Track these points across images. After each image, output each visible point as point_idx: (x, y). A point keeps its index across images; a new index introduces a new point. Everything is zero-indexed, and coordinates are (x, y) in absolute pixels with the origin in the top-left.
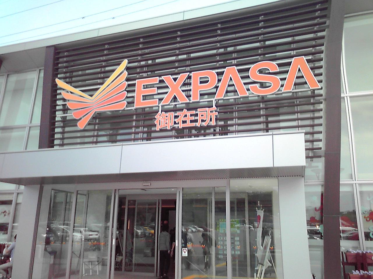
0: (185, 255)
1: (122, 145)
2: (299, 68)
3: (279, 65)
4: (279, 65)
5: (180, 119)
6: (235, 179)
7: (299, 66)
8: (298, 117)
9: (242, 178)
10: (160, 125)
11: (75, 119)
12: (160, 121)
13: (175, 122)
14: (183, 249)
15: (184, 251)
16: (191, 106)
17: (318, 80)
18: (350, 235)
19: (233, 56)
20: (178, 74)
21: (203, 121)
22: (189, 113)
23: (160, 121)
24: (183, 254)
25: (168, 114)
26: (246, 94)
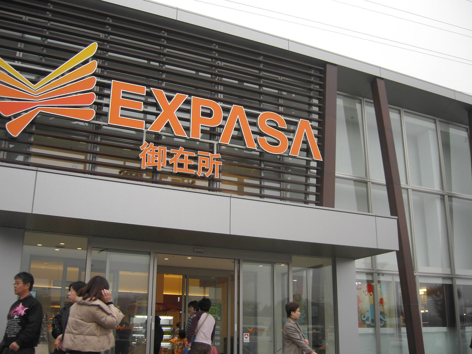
0: (247, 342)
1: (231, 197)
2: (238, 118)
3: (288, 122)
4: (288, 122)
5: (175, 160)
6: (53, 234)
8: (5, 146)
9: (85, 236)
10: (146, 162)
12: (147, 155)
13: (168, 162)
14: (244, 334)
15: (245, 336)
16: (192, 144)
17: (267, 140)
18: (464, 318)
19: (19, 46)
21: (204, 169)
22: (187, 154)
23: (147, 155)
24: (244, 340)
25: (158, 148)
26: (150, 129)
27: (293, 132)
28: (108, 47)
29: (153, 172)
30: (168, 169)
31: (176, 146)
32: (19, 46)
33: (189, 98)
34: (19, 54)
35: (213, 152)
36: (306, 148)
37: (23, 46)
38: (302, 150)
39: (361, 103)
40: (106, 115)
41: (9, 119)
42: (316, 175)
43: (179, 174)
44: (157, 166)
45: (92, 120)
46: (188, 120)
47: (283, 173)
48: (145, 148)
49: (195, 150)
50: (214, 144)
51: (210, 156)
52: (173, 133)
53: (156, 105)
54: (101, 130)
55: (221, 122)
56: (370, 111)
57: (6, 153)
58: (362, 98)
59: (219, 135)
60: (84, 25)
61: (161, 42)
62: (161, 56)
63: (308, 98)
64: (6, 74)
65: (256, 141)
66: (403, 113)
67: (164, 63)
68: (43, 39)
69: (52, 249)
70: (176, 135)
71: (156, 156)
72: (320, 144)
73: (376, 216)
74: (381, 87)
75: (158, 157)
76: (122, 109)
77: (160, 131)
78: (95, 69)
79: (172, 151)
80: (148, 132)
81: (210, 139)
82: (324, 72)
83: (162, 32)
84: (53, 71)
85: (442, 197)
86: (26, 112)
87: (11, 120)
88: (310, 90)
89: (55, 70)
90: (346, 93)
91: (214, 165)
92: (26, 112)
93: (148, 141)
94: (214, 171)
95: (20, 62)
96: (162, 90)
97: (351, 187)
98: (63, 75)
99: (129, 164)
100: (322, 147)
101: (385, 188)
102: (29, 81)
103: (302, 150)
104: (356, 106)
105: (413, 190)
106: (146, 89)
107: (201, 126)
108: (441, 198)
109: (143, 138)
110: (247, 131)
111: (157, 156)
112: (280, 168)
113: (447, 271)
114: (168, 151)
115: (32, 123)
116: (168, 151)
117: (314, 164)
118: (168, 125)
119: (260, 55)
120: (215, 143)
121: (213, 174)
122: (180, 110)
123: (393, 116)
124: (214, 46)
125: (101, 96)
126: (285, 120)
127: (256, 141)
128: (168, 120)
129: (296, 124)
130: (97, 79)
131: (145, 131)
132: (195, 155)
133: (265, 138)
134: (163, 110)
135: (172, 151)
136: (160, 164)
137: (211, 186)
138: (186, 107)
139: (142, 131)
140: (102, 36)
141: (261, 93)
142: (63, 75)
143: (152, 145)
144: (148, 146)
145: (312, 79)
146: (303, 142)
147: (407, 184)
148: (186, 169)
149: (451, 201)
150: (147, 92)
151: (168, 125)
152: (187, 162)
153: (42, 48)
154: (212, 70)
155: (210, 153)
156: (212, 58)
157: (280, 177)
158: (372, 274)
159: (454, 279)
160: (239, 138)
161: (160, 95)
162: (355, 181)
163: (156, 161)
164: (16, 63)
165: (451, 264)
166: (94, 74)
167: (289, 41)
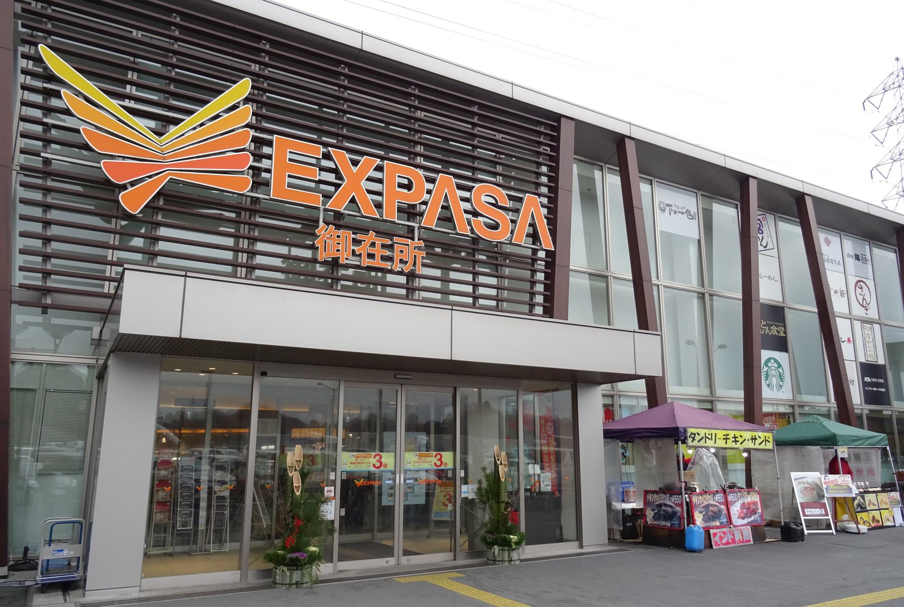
7: (446, 190)
10: (325, 251)
11: (108, 181)
12: (325, 241)
13: (353, 251)
20: (362, 154)
21: (401, 261)
22: (379, 242)
23: (325, 241)
25: (340, 232)
27: (517, 211)
28: (265, 85)
29: (333, 265)
30: (354, 261)
31: (366, 231)
32: (130, 76)
33: (381, 163)
34: (129, 89)
35: (413, 239)
36: (532, 233)
37: (135, 78)
38: (528, 235)
39: (602, 170)
40: (267, 184)
41: (124, 187)
42: (543, 268)
43: (370, 268)
44: (339, 257)
45: (248, 191)
46: (380, 194)
47: (501, 265)
48: (323, 232)
49: (390, 235)
50: (414, 227)
51: (409, 243)
52: (359, 211)
53: (335, 171)
54: (259, 204)
55: (426, 197)
56: (614, 181)
57: (117, 236)
58: (603, 164)
59: (421, 214)
60: (230, 51)
61: (340, 81)
62: (341, 101)
63: (535, 165)
64: (114, 119)
65: (469, 224)
66: (655, 184)
67: (345, 112)
68: (168, 68)
69: (195, 374)
70: (364, 215)
71: (337, 243)
72: (551, 227)
73: (634, 332)
74: (631, 149)
75: (340, 245)
76: (289, 176)
77: (343, 208)
78: (250, 118)
79: (359, 237)
80: (326, 210)
81: (408, 220)
82: (557, 129)
83: (340, 66)
84: (188, 119)
85: (701, 296)
86: (150, 177)
87: (126, 189)
88: (539, 154)
89: (190, 116)
90: (587, 158)
91: (415, 256)
92: (150, 177)
93: (327, 223)
94: (415, 264)
95: (133, 102)
96: (345, 152)
97: (585, 282)
98: (202, 125)
99: (296, 252)
100: (553, 233)
101: (632, 284)
102: (151, 131)
103: (528, 235)
104: (594, 172)
105: (665, 287)
106: (322, 149)
107: (398, 202)
108: (698, 297)
109: (319, 219)
110: (459, 208)
111: (339, 244)
112: (497, 259)
113: (705, 392)
114: (354, 236)
115: (159, 194)
116: (354, 236)
117: (542, 254)
118: (353, 201)
119: (473, 103)
120: (416, 225)
121: (413, 268)
122: (369, 179)
123: (645, 188)
124: (412, 89)
125: (258, 157)
126: (507, 195)
127: (469, 224)
128: (354, 194)
129: (520, 200)
130: (252, 133)
131: (322, 208)
132: (390, 242)
133: (480, 218)
134: (345, 179)
135: (359, 237)
136: (343, 255)
137: (410, 284)
138: (378, 175)
139: (318, 209)
140: (255, 68)
141: (474, 158)
142: (202, 125)
143: (331, 228)
144: (327, 229)
145: (542, 140)
146: (530, 225)
147: (658, 279)
148: (378, 260)
149: (711, 300)
150: (323, 154)
151: (353, 201)
152: (379, 252)
153: (167, 81)
154: (411, 123)
155: (410, 240)
156: (410, 106)
157: (497, 271)
158: (612, 396)
159: (714, 402)
160: (446, 219)
161: (341, 158)
162: (590, 274)
163: (338, 251)
164: (127, 103)
165: (711, 385)
166: (247, 126)
167: (512, 84)
